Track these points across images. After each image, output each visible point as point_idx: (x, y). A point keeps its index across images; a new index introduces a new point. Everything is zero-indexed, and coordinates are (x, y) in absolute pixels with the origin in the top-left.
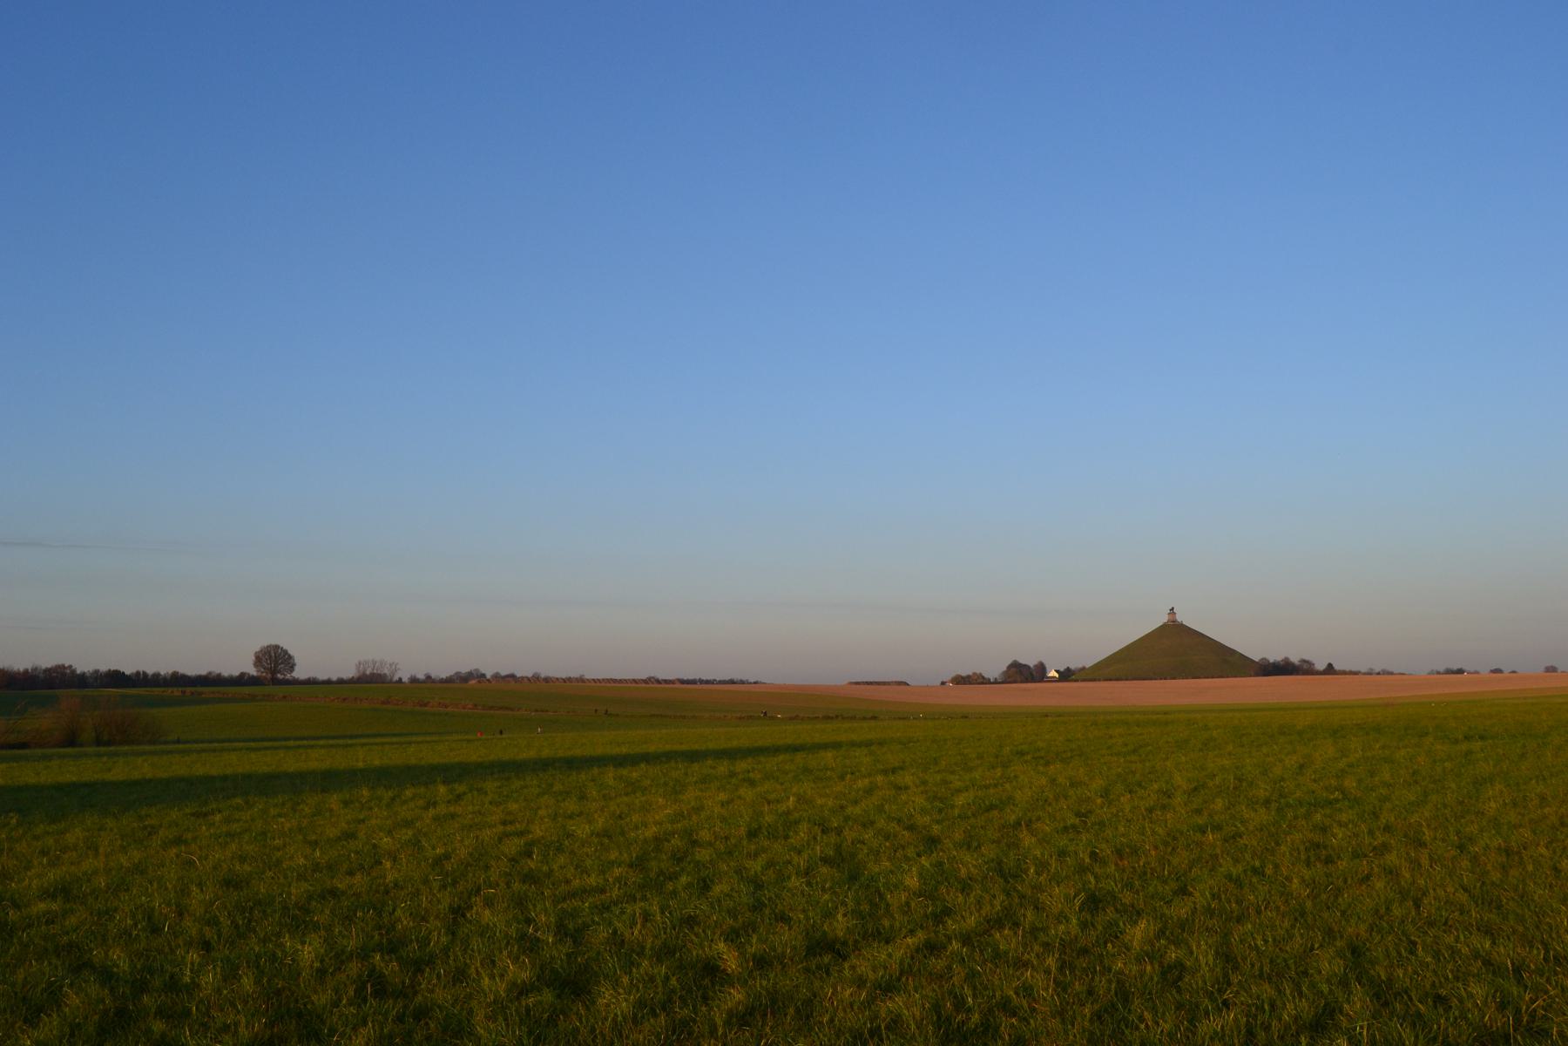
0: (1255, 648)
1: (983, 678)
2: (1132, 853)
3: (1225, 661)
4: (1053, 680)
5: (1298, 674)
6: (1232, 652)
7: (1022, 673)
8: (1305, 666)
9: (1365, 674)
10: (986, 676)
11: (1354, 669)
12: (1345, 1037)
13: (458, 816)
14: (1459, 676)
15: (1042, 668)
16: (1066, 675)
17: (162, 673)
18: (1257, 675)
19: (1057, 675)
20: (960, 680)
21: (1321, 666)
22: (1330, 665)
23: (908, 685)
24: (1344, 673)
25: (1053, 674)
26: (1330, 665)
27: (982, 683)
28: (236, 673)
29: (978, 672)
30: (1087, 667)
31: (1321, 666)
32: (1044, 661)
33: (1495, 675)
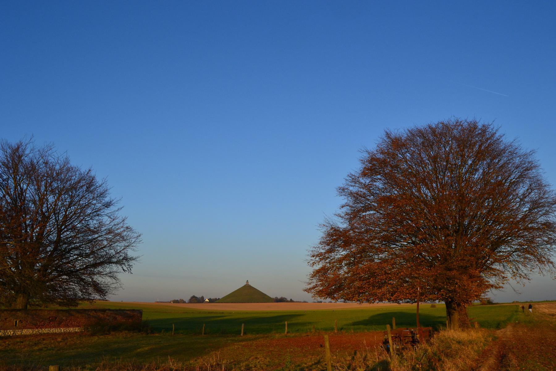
0: (272, 294)
1: (183, 301)
2: (515, 323)
3: (263, 298)
4: (207, 302)
5: (284, 302)
6: (265, 295)
7: (195, 300)
8: (285, 299)
9: (302, 302)
10: (184, 300)
11: (300, 301)
12: (360, 286)
13: (385, 130)
14: (320, 303)
15: (203, 298)
16: (211, 301)
17: (279, 298)
18: (275, 302)
19: (208, 301)
20: (176, 302)
21: (289, 299)
22: (291, 299)
23: (308, 302)
24: (297, 302)
25: (207, 300)
26: (291, 299)
27: (183, 303)
28: (274, 297)
29: (182, 299)
30: (220, 298)
31: (289, 299)
32: (204, 296)
33: (329, 303)
